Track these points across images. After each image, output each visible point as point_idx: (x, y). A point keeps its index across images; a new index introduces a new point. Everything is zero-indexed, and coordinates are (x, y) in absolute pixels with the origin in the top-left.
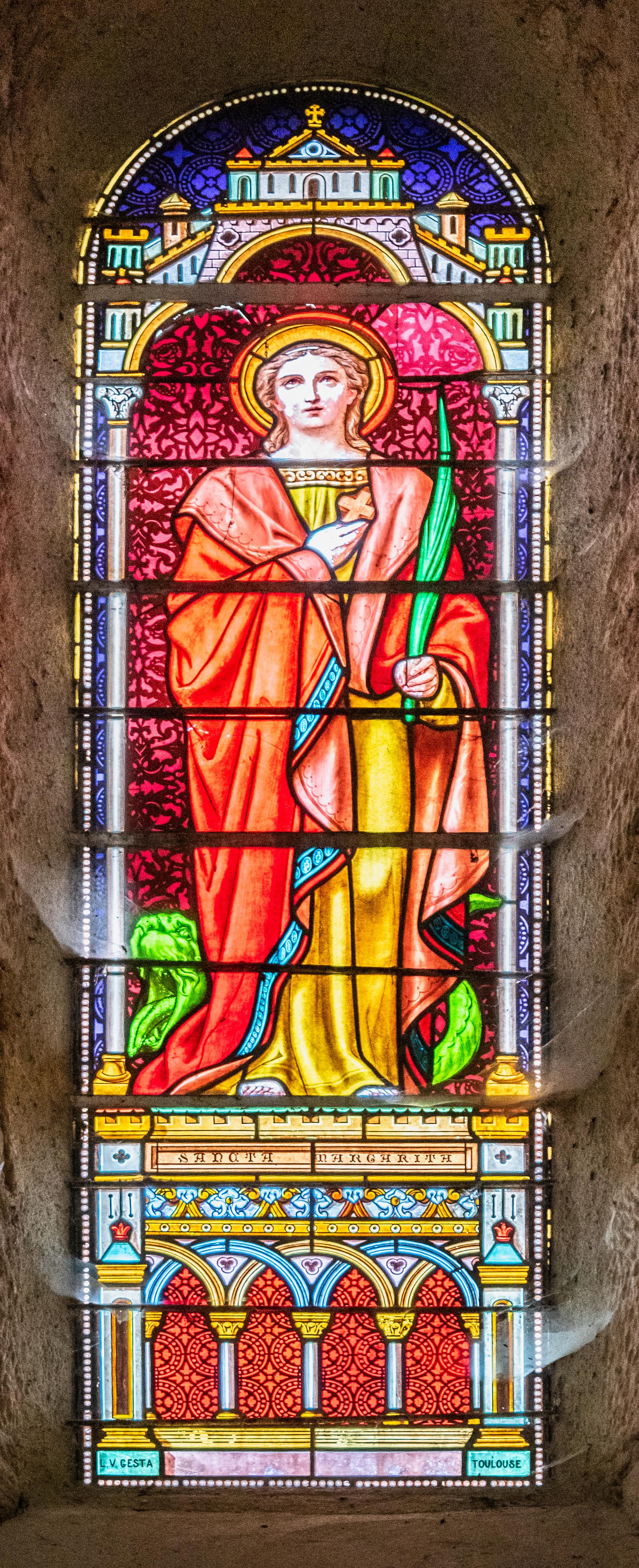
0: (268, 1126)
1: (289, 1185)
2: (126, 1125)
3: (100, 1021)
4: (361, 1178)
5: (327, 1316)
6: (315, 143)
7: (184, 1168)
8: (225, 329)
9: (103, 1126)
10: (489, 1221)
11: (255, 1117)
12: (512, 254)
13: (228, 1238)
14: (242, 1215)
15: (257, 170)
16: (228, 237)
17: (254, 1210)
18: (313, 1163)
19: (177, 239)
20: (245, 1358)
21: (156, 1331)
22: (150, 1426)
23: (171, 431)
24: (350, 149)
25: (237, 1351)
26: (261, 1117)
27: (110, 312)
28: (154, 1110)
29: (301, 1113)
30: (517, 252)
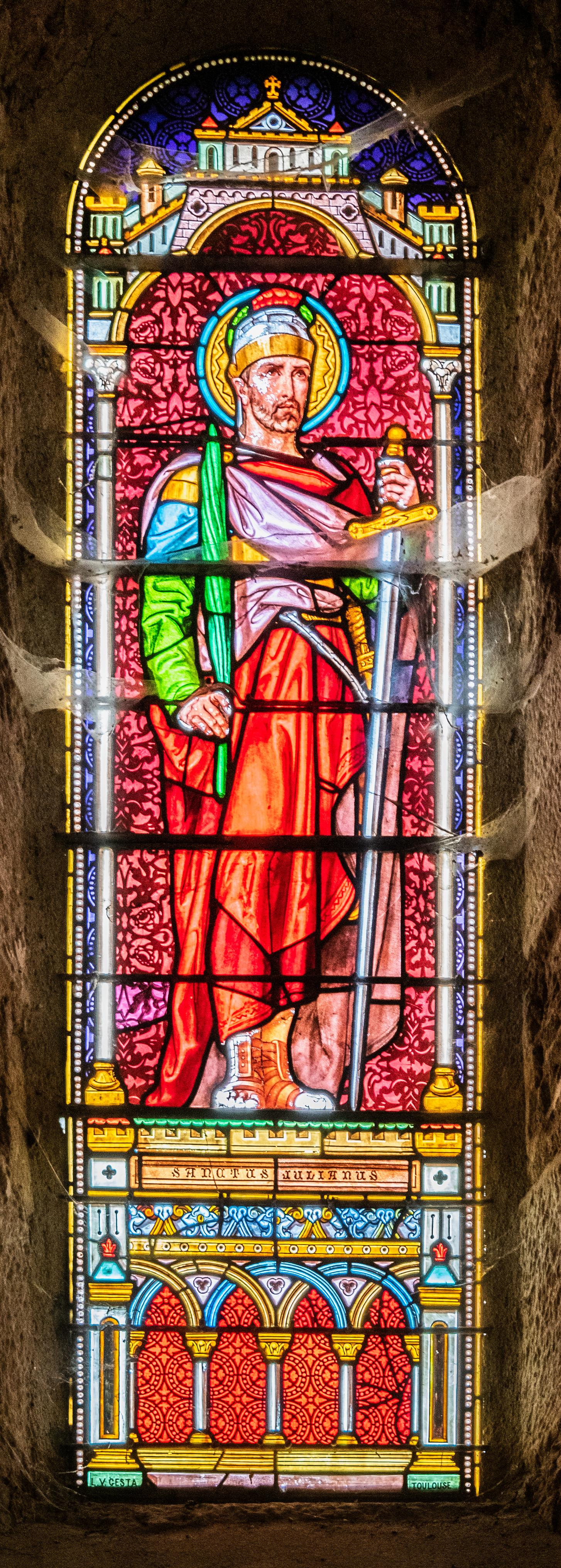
2: (114, 1138)
4: (318, 1197)
5: (361, 1337)
6: (273, 116)
8: (391, 301)
16: (197, 207)
21: (139, 1350)
23: (351, 410)
24: (304, 124)
25: (282, 1372)
27: (96, 280)
28: (138, 1121)
29: (267, 1127)
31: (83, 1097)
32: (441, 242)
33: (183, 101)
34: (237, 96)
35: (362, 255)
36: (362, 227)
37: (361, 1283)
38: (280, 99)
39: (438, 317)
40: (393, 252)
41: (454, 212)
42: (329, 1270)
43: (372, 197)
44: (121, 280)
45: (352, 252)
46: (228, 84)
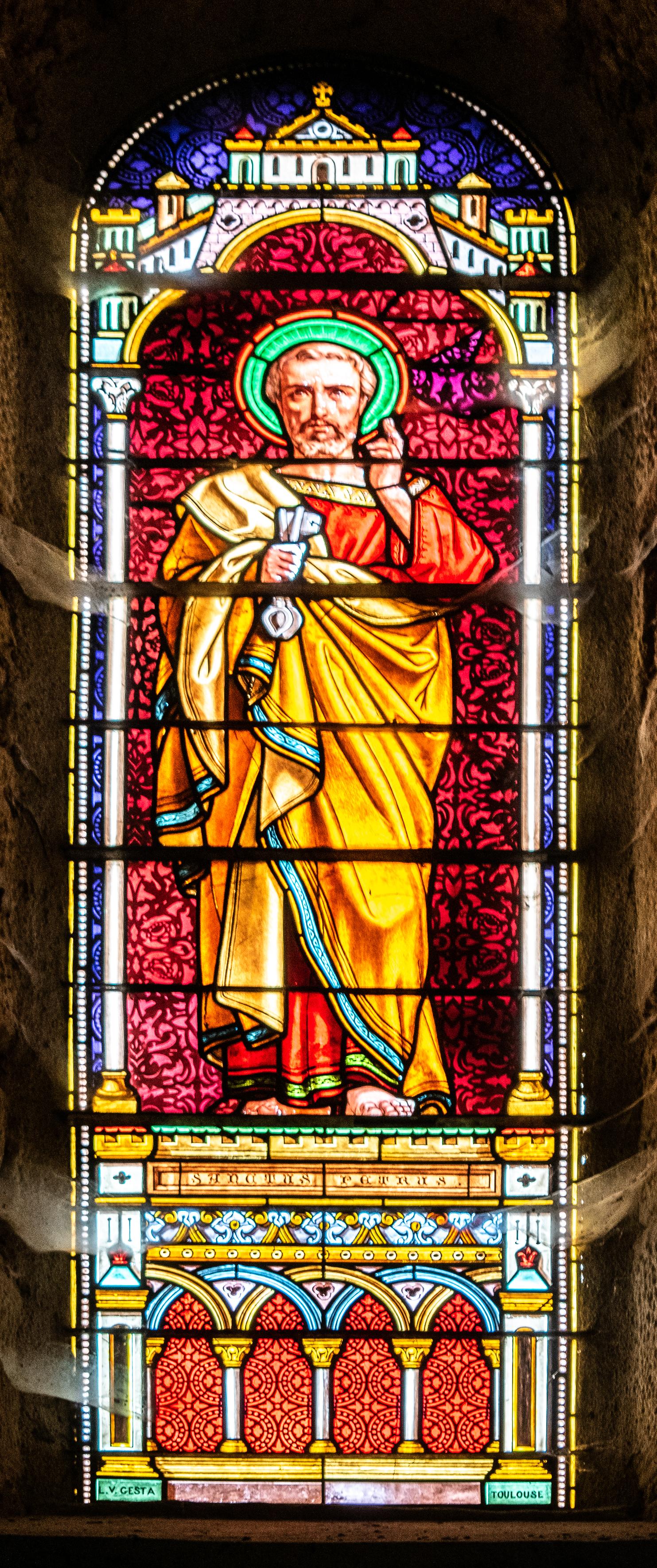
0: (280, 1146)
1: (300, 1210)
2: (128, 1144)
3: (97, 790)
4: (378, 1202)
10: (512, 1249)
16: (228, 220)
17: (441, 1236)
20: (251, 1385)
21: (157, 1357)
22: (152, 1455)
23: (170, 438)
24: (359, 129)
25: (332, 1378)
28: (156, 1129)
30: (541, 235)
31: (90, 1102)
32: (531, 249)
33: (212, 111)
34: (279, 104)
35: (433, 270)
36: (433, 237)
39: (526, 336)
40: (471, 264)
41: (549, 218)
43: (445, 203)
44: (135, 300)
45: (419, 268)
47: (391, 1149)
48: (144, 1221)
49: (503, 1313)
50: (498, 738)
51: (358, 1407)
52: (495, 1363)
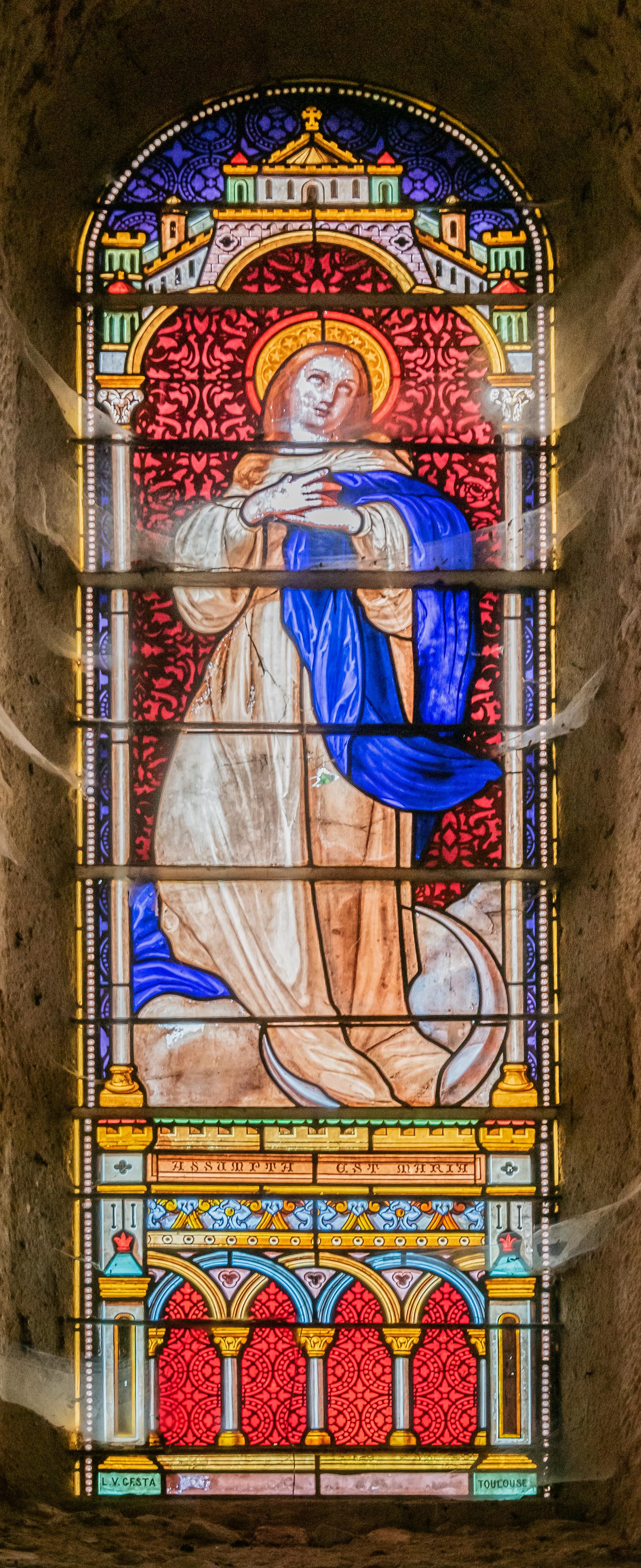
4: (366, 1190)
5: (418, 1332)
7: (401, 1179)
9: (105, 1138)
10: (494, 1233)
11: (260, 1128)
12: (127, 260)
13: (404, 1251)
14: (243, 1226)
15: (255, 176)
16: (227, 242)
17: (425, 1222)
18: (315, 1173)
19: (175, 242)
21: (159, 1350)
24: (347, 155)
26: (266, 1129)
30: (518, 254)
32: (508, 266)
37: (416, 1275)
38: (321, 130)
39: (508, 348)
40: (453, 281)
41: (522, 237)
42: (378, 1262)
46: (260, 118)
47: (382, 1140)
48: (146, 1210)
49: (488, 1300)
50: (164, 433)
51: (351, 1396)
52: (481, 1350)
